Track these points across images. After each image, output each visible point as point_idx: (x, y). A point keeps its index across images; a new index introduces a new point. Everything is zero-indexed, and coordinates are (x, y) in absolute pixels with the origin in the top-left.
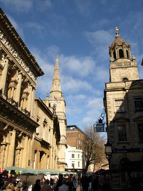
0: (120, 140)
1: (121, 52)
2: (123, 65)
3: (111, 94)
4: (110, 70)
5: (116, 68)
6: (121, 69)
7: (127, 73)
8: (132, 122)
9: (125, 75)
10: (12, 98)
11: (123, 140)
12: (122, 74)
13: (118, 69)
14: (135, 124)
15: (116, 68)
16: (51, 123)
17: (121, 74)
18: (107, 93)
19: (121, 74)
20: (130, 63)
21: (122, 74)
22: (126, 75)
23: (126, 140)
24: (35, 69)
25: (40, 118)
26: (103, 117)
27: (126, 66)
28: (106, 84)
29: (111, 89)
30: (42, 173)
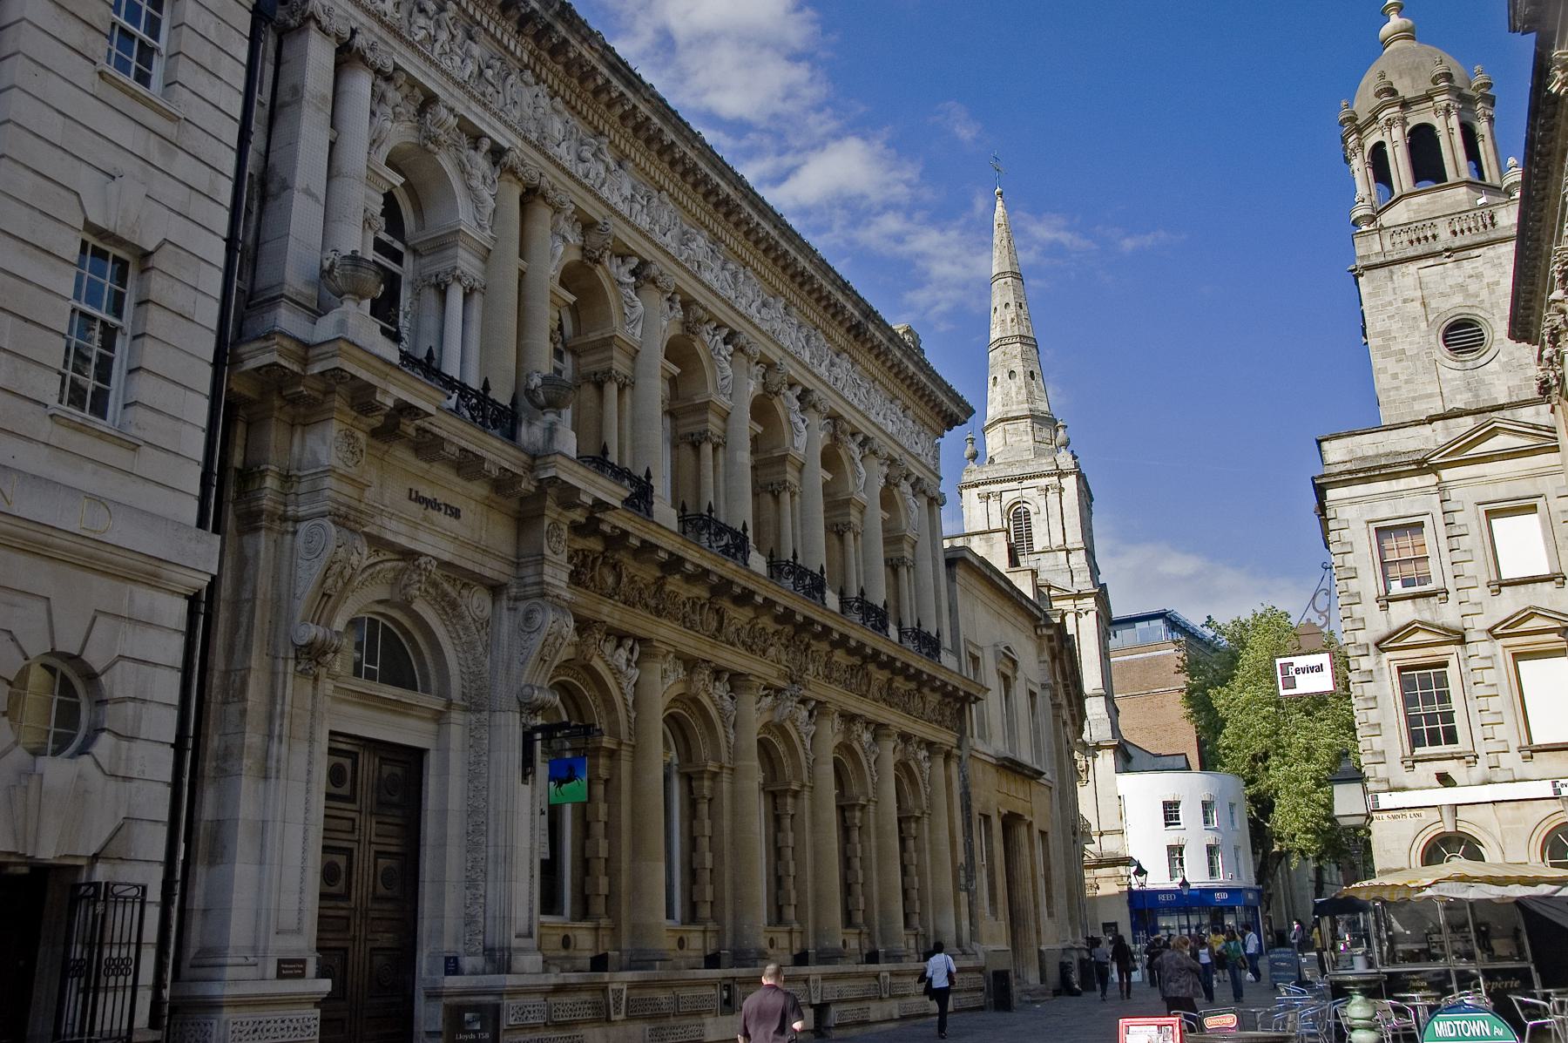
0: (1416, 740)
1: (1423, 144)
2: (1445, 237)
3: (1353, 501)
4: (1356, 277)
5: (1394, 263)
6: (1431, 262)
7: (1473, 287)
8: (1482, 647)
9: (1458, 299)
10: (862, 593)
11: (1434, 741)
12: (1442, 295)
13: (1412, 267)
14: (1500, 650)
15: (1394, 263)
16: (1032, 665)
17: (1432, 296)
18: (1332, 494)
19: (1432, 296)
20: (1492, 218)
21: (1442, 295)
22: (1468, 296)
23: (1451, 737)
24: (899, 372)
25: (981, 649)
26: (1322, 613)
27: (1467, 239)
28: (1319, 442)
29: (1350, 472)
30: (113, 716)
